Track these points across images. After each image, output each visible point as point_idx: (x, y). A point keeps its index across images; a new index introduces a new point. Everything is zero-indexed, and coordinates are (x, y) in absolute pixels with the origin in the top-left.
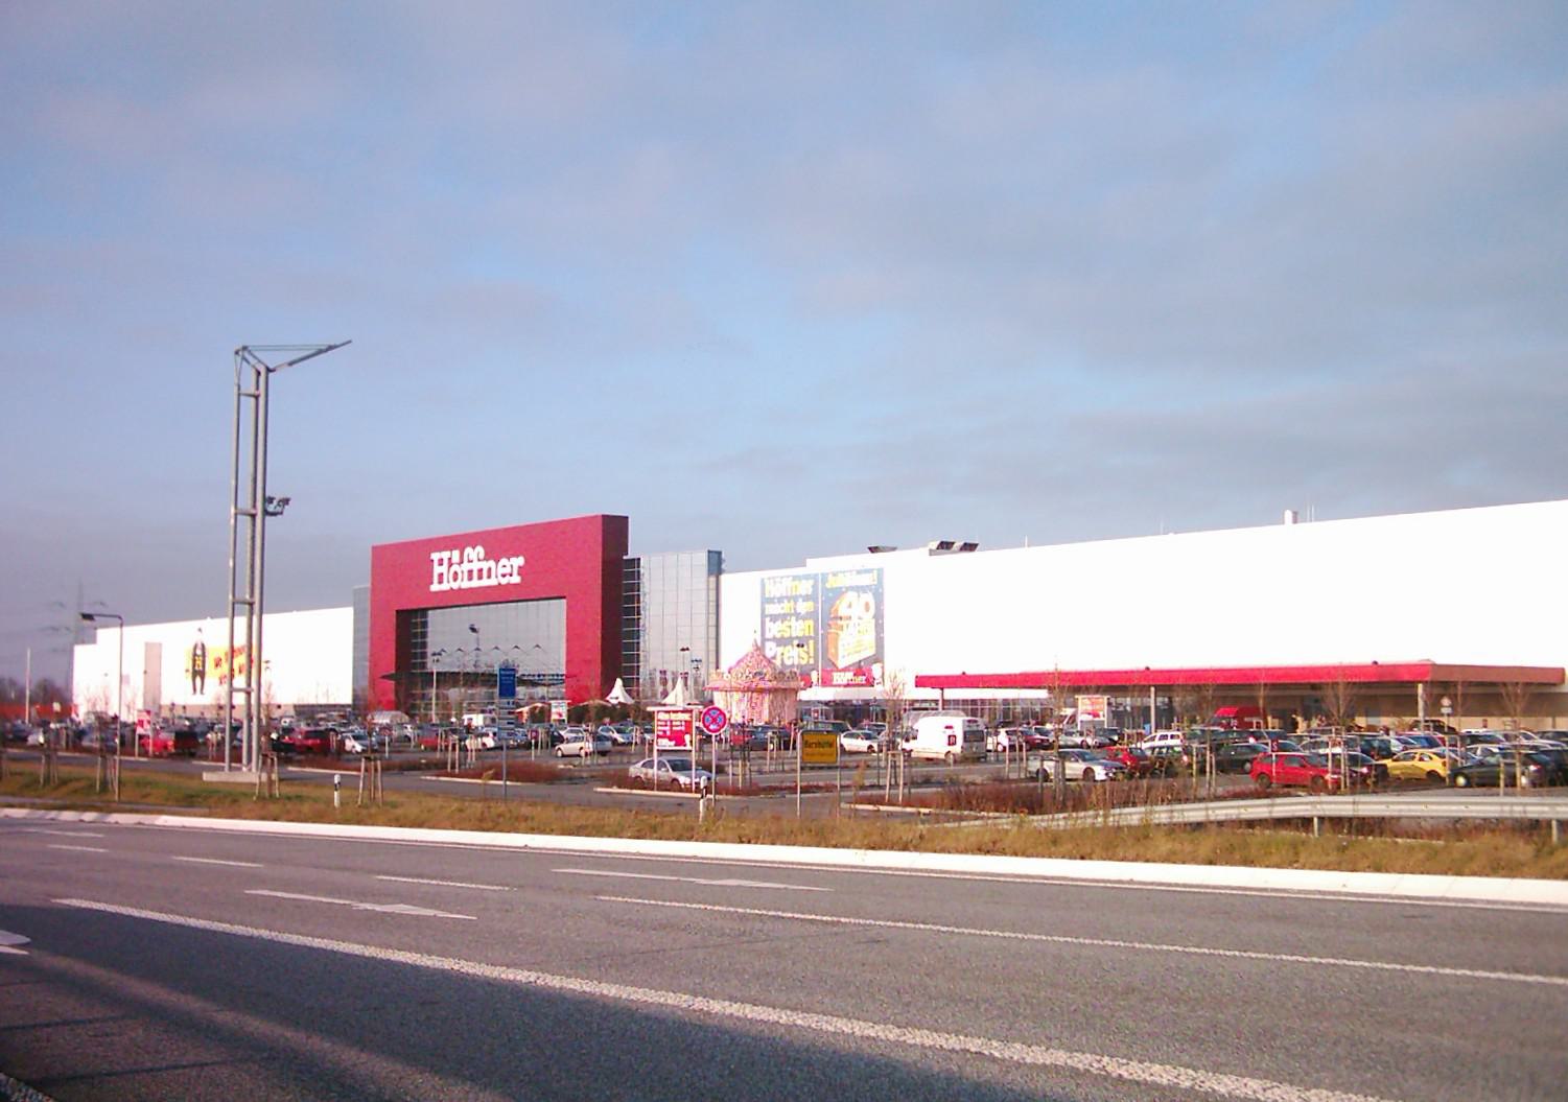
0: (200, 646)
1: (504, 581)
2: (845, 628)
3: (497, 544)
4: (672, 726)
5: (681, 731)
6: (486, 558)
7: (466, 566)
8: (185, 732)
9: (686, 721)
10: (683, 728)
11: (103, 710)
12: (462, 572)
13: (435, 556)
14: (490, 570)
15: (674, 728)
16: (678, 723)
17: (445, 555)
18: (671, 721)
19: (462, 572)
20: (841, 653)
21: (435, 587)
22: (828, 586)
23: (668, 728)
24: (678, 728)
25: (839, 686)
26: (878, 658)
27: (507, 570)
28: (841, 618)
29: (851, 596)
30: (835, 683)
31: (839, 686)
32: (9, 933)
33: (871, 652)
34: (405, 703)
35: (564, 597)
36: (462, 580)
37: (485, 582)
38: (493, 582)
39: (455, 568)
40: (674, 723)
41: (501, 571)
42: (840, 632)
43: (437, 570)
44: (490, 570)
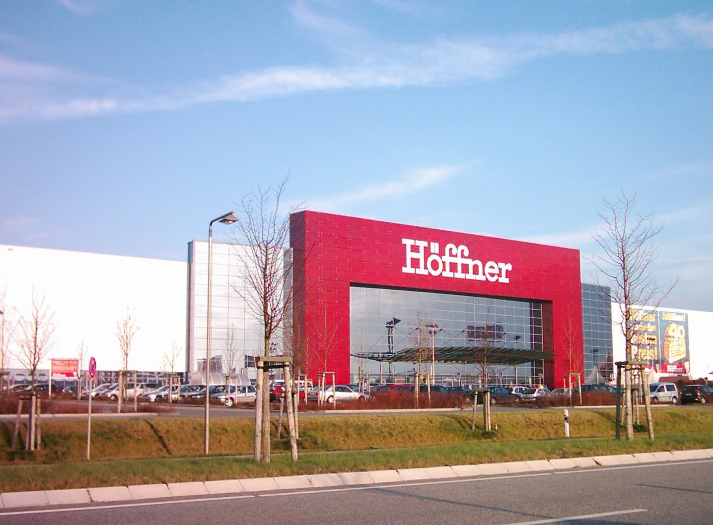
2: (672, 342)
6: (472, 256)
13: (408, 242)
20: (670, 355)
21: (408, 269)
26: (687, 359)
27: (496, 271)
28: (669, 336)
29: (674, 326)
30: (668, 371)
33: (684, 356)
36: (444, 270)
37: (470, 276)
38: (480, 277)
42: (670, 344)
43: (410, 255)
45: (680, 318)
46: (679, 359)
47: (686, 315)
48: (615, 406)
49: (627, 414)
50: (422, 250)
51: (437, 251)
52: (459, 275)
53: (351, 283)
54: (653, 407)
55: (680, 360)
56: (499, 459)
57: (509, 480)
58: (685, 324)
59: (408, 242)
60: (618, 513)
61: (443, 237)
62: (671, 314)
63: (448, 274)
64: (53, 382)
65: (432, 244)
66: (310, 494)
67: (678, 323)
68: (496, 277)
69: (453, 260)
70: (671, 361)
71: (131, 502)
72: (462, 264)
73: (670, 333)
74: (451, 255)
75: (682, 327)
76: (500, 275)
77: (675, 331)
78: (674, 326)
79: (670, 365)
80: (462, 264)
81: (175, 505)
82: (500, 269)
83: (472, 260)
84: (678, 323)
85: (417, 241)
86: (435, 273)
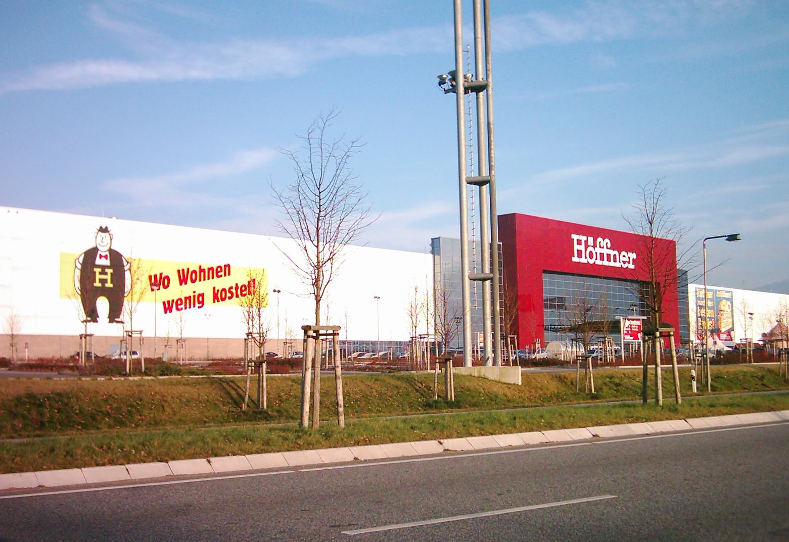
0: (234, 286)
1: (625, 266)
3: (620, 241)
4: (631, 328)
5: (636, 331)
6: (612, 248)
7: (598, 250)
8: (674, 263)
9: (638, 326)
10: (637, 330)
11: (175, 356)
12: (596, 253)
13: (575, 237)
14: (615, 256)
15: (633, 329)
16: (634, 327)
17: (583, 238)
18: (631, 325)
19: (596, 253)
20: (723, 326)
21: (575, 259)
22: (717, 296)
23: (629, 329)
24: (635, 329)
25: (723, 340)
26: (732, 329)
27: (626, 259)
28: (721, 310)
29: (724, 301)
31: (723, 340)
32: (310, 464)
33: (730, 326)
34: (531, 388)
35: (316, 325)
36: (596, 259)
37: (612, 264)
38: (618, 265)
39: (590, 249)
40: (633, 327)
41: (622, 259)
43: (577, 247)
44: (615, 256)
45: (727, 295)
46: (728, 329)
47: (732, 292)
48: (642, 367)
49: (590, 372)
50: (583, 243)
51: (592, 245)
52: (605, 263)
53: (543, 270)
54: (664, 368)
55: (729, 330)
56: (626, 421)
57: (125, 493)
58: (730, 300)
59: (575, 237)
60: (530, 509)
61: (595, 232)
62: (723, 291)
63: (599, 262)
64: (581, 367)
65: (589, 238)
66: (381, 465)
67: (727, 299)
68: (627, 264)
69: (602, 251)
70: (723, 330)
71: (63, 489)
72: (581, 245)
73: (722, 308)
74: (600, 247)
75: (729, 303)
76: (629, 263)
77: (725, 305)
78: (724, 301)
79: (722, 333)
80: (581, 245)
81: (173, 486)
82: (629, 258)
83: (612, 250)
84: (727, 299)
85: (580, 236)
86: (592, 261)
